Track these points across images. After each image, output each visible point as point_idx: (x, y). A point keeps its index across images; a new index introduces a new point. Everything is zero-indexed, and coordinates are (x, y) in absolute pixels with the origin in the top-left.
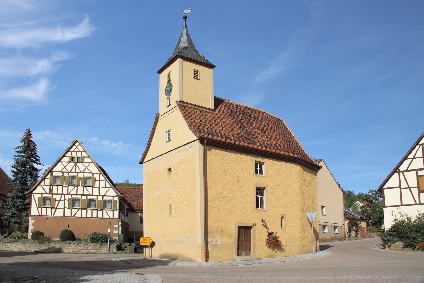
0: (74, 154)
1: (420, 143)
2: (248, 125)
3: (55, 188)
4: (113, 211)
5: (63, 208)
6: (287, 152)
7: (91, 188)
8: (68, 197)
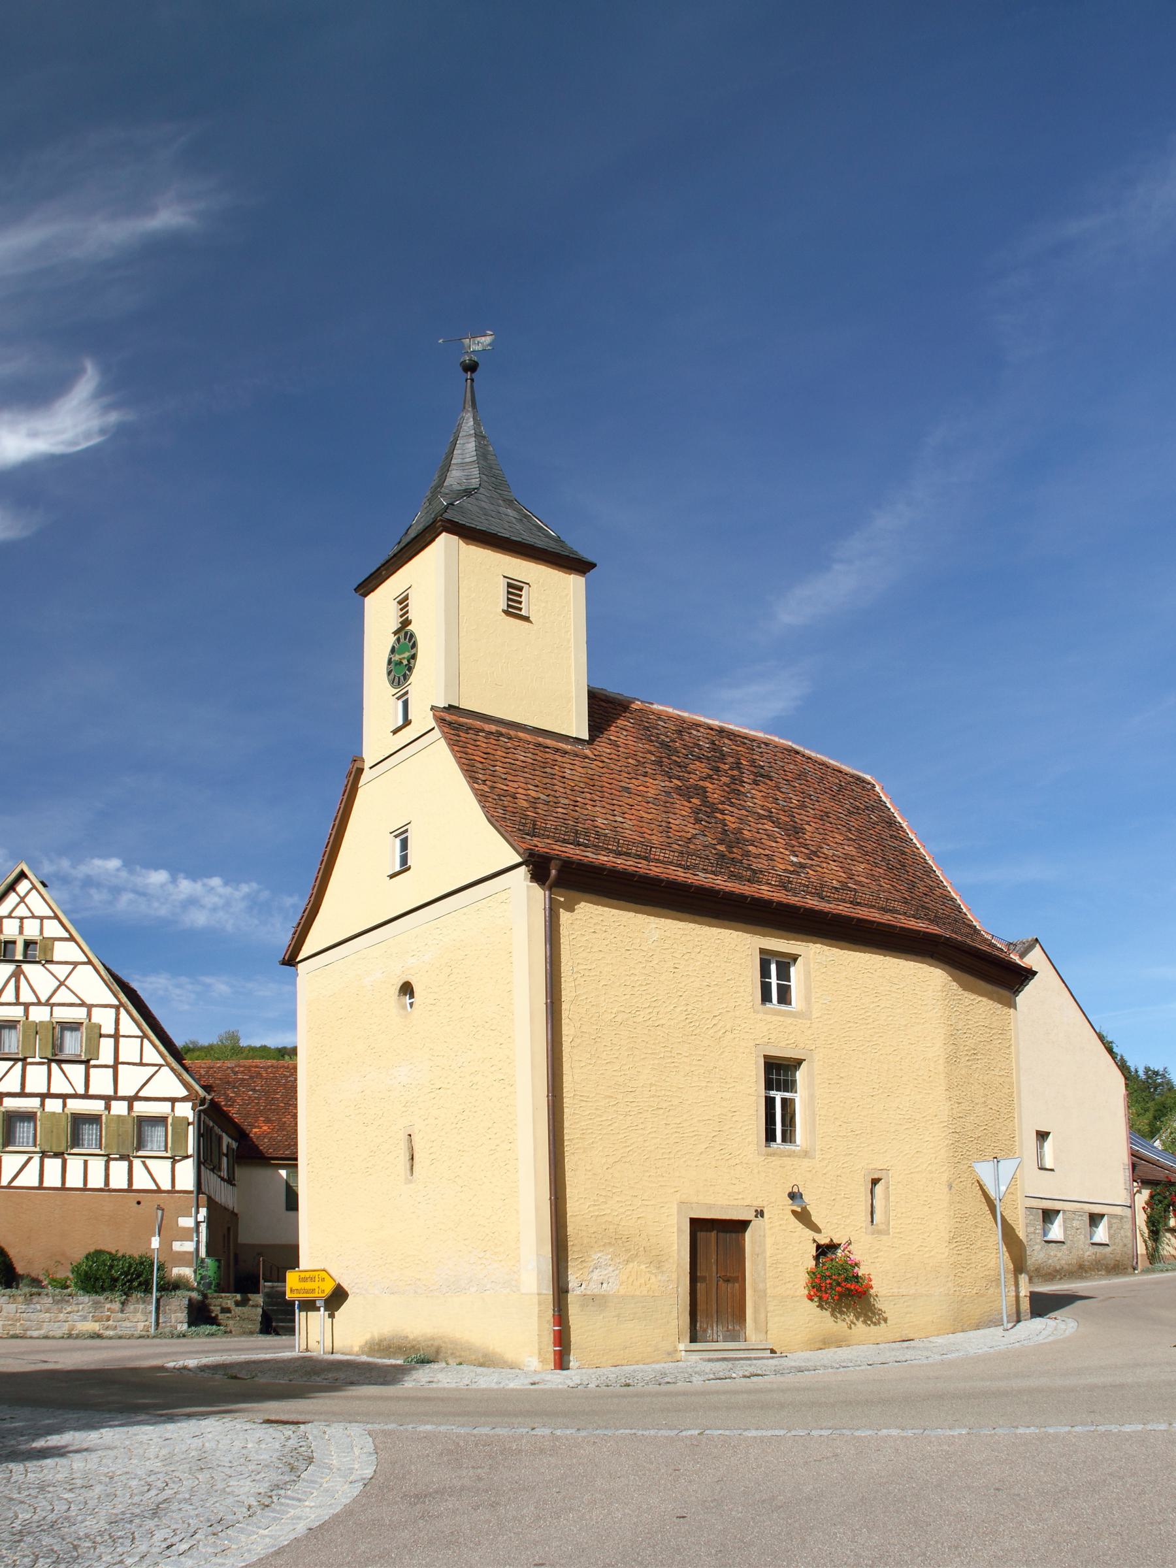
7: (82, 1067)
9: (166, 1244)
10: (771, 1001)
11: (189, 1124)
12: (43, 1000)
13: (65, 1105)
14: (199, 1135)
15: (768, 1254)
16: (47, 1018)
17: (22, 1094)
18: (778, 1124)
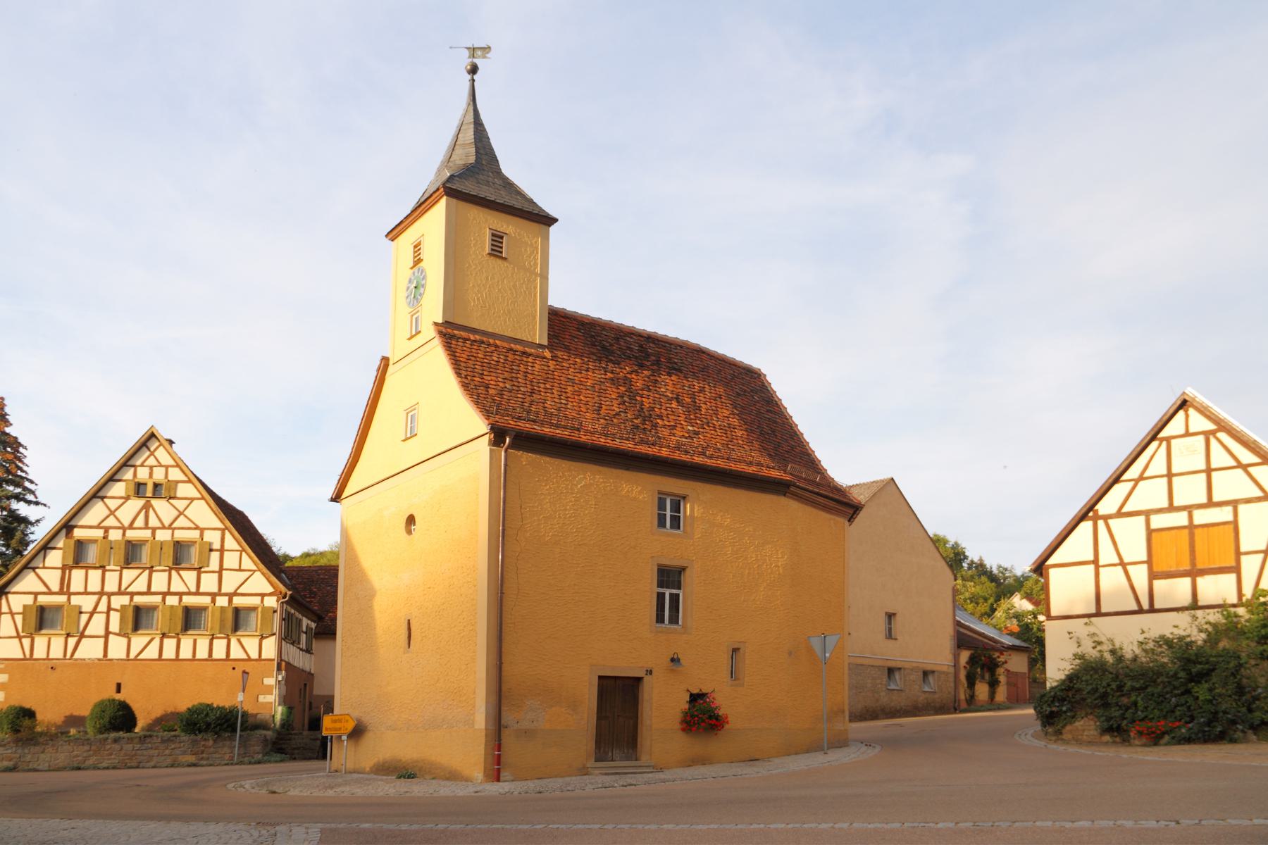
0: (143, 474)
1: (1161, 435)
2: (649, 390)
3: (77, 575)
4: (262, 638)
5: (102, 633)
6: (759, 464)
7: (195, 573)
8: (118, 602)
10: (664, 526)
12: (167, 524)
13: (181, 600)
16: (169, 538)
17: (149, 592)
18: (667, 611)
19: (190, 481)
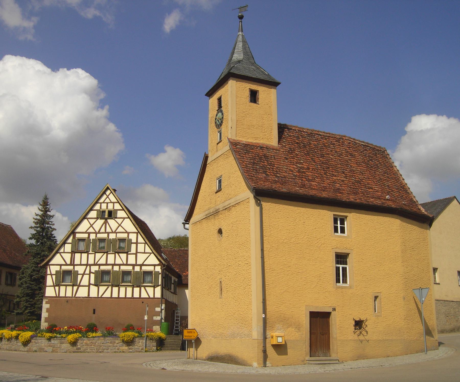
3: (77, 256)
7: (126, 254)
9: (150, 318)
11: (160, 274)
12: (114, 231)
13: (120, 268)
14: (163, 278)
15: (337, 324)
16: (115, 237)
17: (106, 264)
18: (340, 276)
19: (123, 210)
